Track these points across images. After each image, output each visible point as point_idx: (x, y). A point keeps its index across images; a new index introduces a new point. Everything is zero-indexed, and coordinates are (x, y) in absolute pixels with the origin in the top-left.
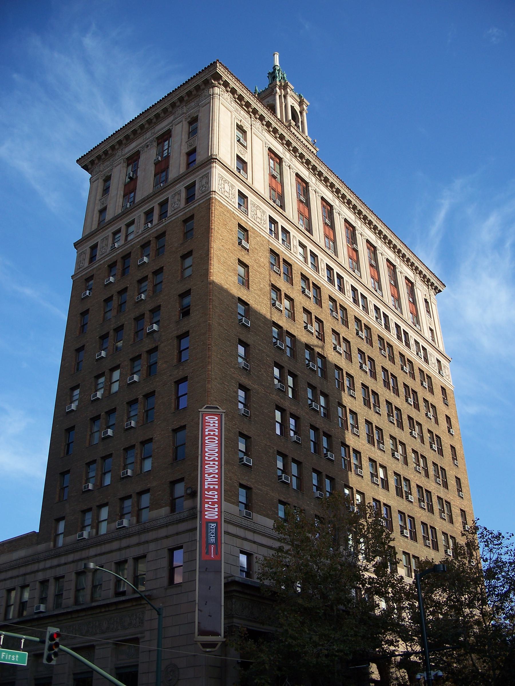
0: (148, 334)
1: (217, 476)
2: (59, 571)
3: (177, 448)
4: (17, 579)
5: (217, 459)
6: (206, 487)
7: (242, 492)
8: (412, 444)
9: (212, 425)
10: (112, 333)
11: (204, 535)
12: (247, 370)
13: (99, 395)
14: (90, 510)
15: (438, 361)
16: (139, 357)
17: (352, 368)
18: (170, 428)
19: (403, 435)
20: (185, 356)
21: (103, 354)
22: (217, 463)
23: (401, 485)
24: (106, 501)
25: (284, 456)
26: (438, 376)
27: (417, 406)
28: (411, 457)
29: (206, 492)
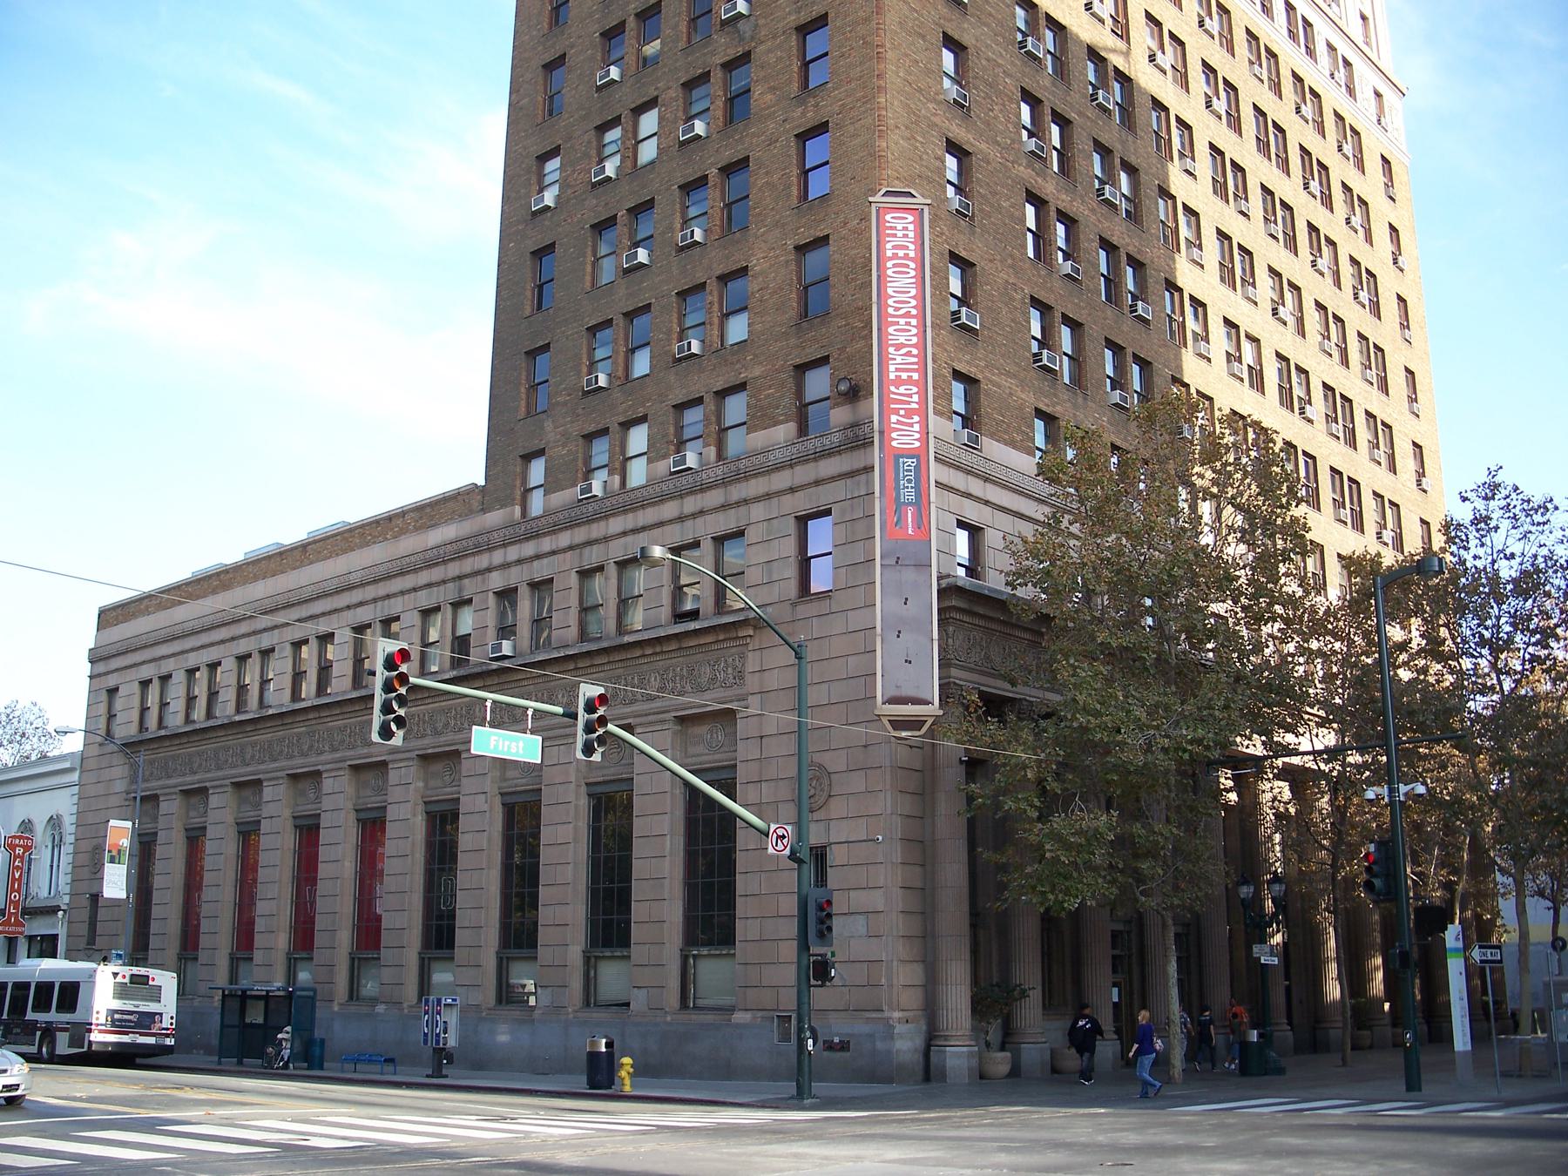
0: (724, 23)
1: (915, 352)
2: (540, 570)
3: (806, 288)
4: (442, 588)
5: (914, 312)
6: (892, 376)
7: (958, 388)
8: (1316, 288)
9: (900, 234)
10: (631, 23)
11: (890, 483)
12: (963, 106)
13: (610, 169)
14: (604, 432)
15: (1378, 95)
16: (704, 78)
17: (1187, 105)
18: (790, 244)
19: (1296, 268)
20: (816, 75)
21: (614, 73)
22: (914, 322)
23: (1290, 382)
24: (641, 412)
25: (1044, 308)
26: (1376, 129)
27: (1327, 201)
28: (1312, 318)
29: (892, 388)
